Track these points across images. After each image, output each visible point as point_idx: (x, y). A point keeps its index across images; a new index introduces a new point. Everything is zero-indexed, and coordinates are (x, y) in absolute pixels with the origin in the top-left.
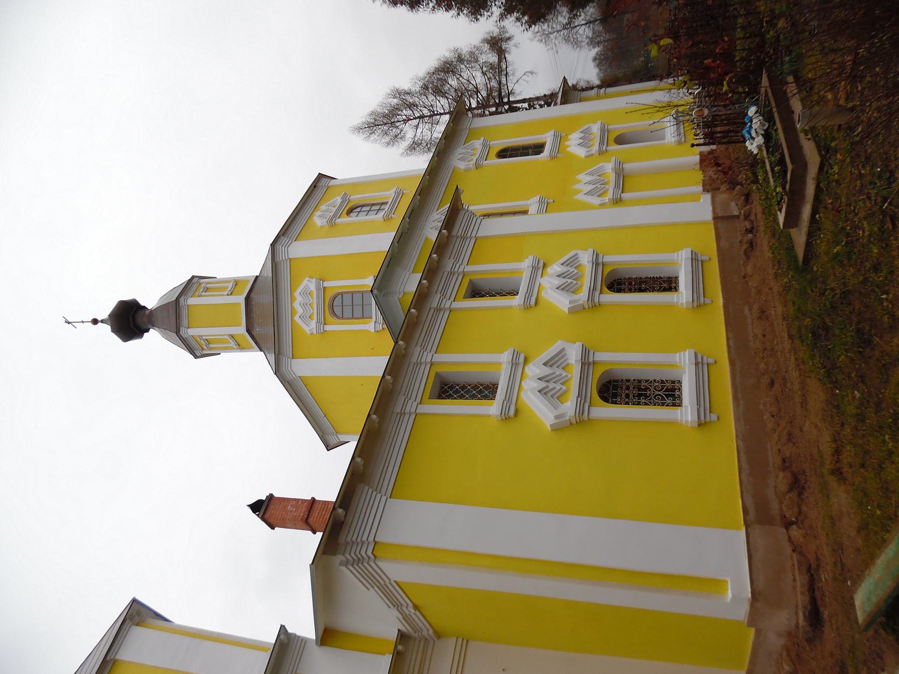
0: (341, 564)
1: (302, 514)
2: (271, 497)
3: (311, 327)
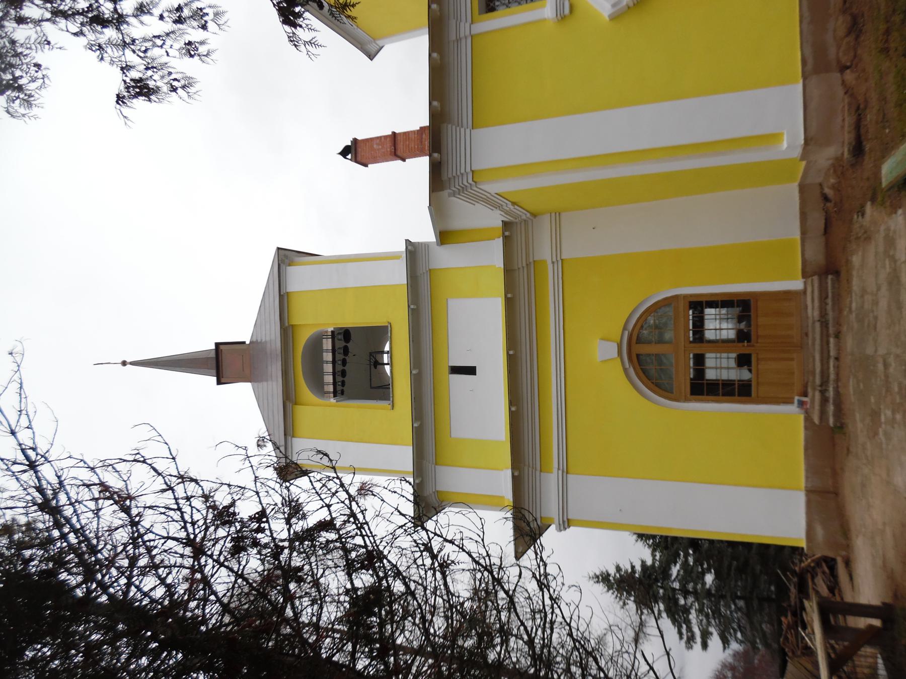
0: (450, 195)
1: (389, 150)
2: (355, 141)
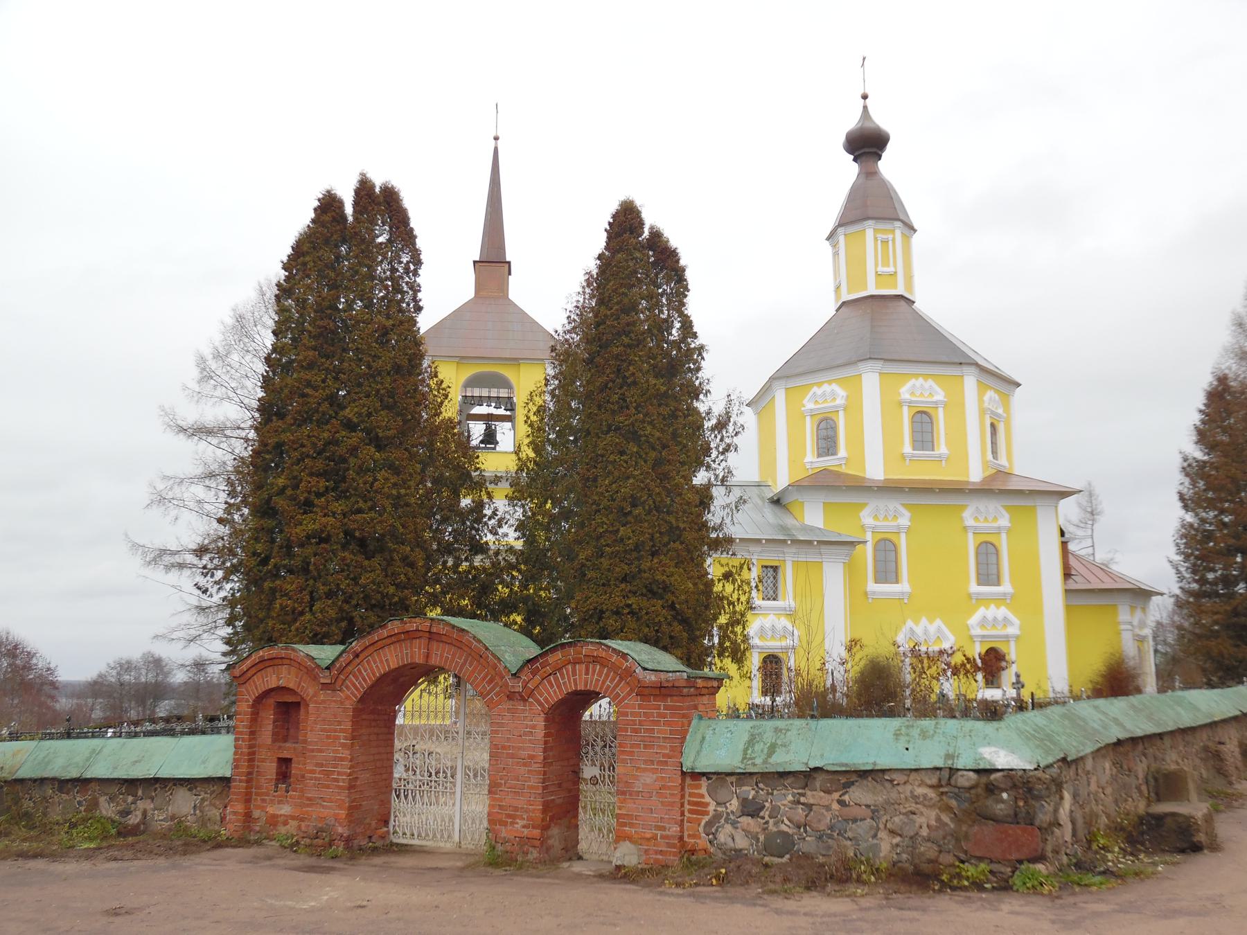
3: (905, 392)
